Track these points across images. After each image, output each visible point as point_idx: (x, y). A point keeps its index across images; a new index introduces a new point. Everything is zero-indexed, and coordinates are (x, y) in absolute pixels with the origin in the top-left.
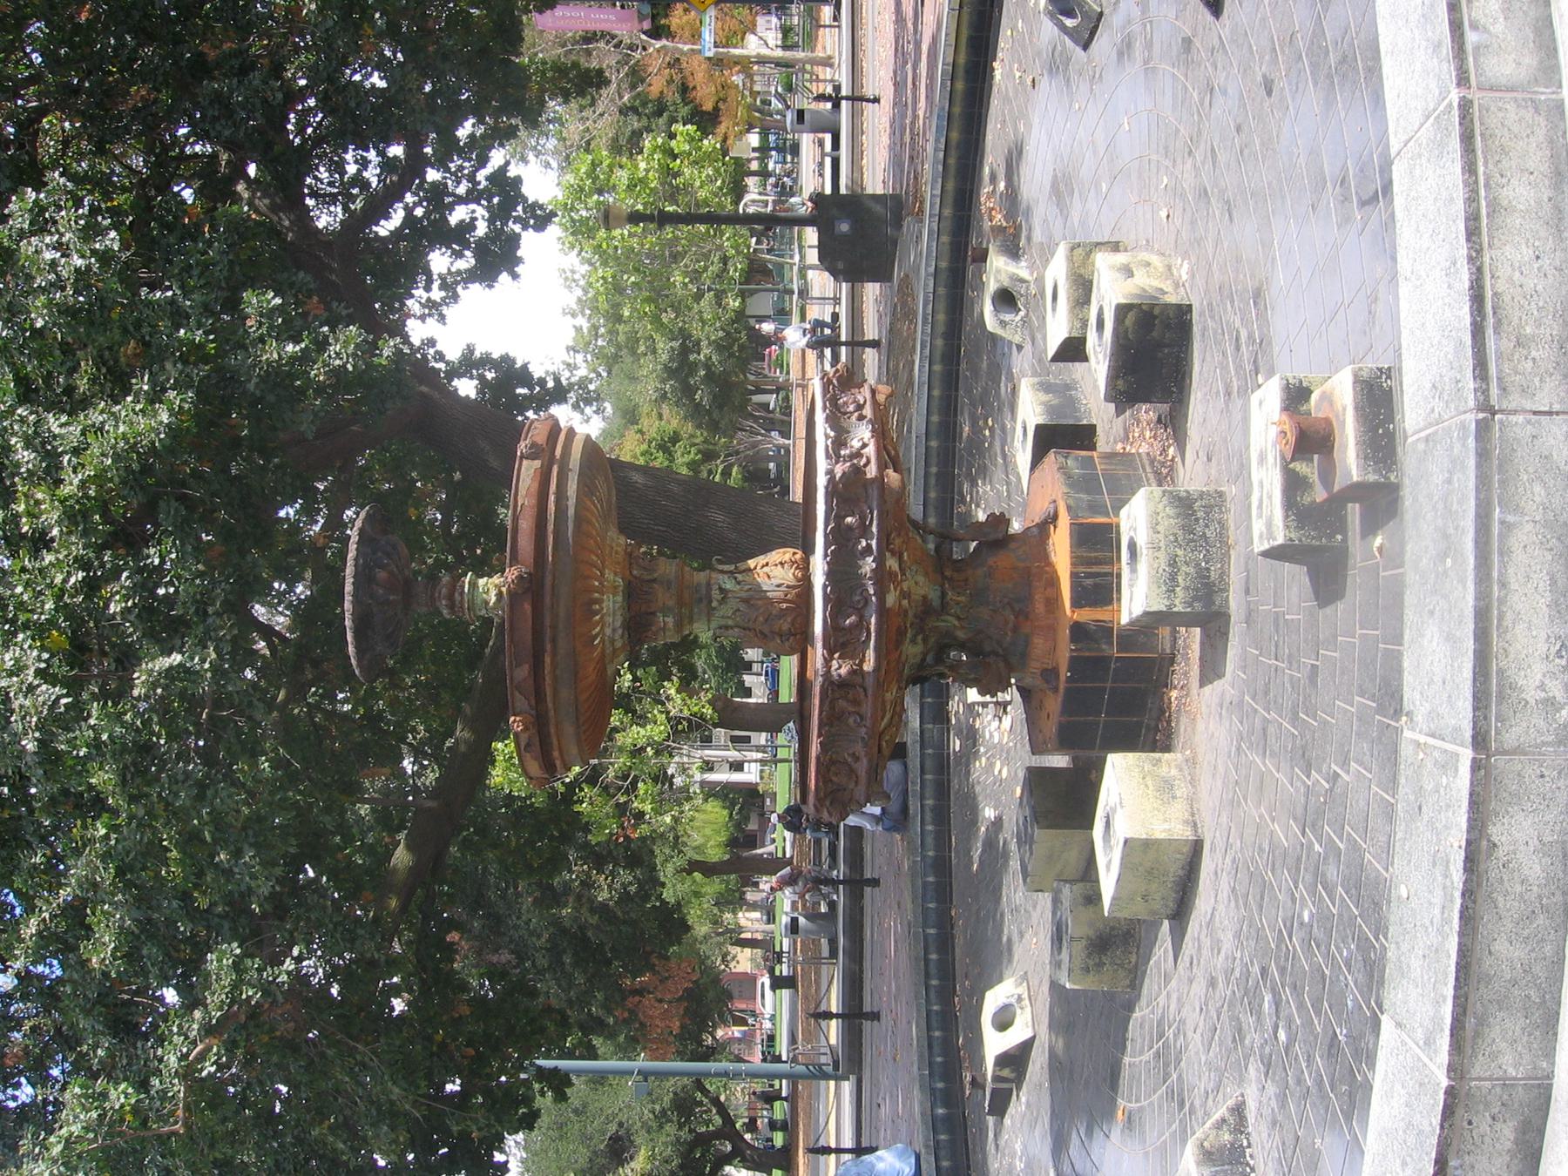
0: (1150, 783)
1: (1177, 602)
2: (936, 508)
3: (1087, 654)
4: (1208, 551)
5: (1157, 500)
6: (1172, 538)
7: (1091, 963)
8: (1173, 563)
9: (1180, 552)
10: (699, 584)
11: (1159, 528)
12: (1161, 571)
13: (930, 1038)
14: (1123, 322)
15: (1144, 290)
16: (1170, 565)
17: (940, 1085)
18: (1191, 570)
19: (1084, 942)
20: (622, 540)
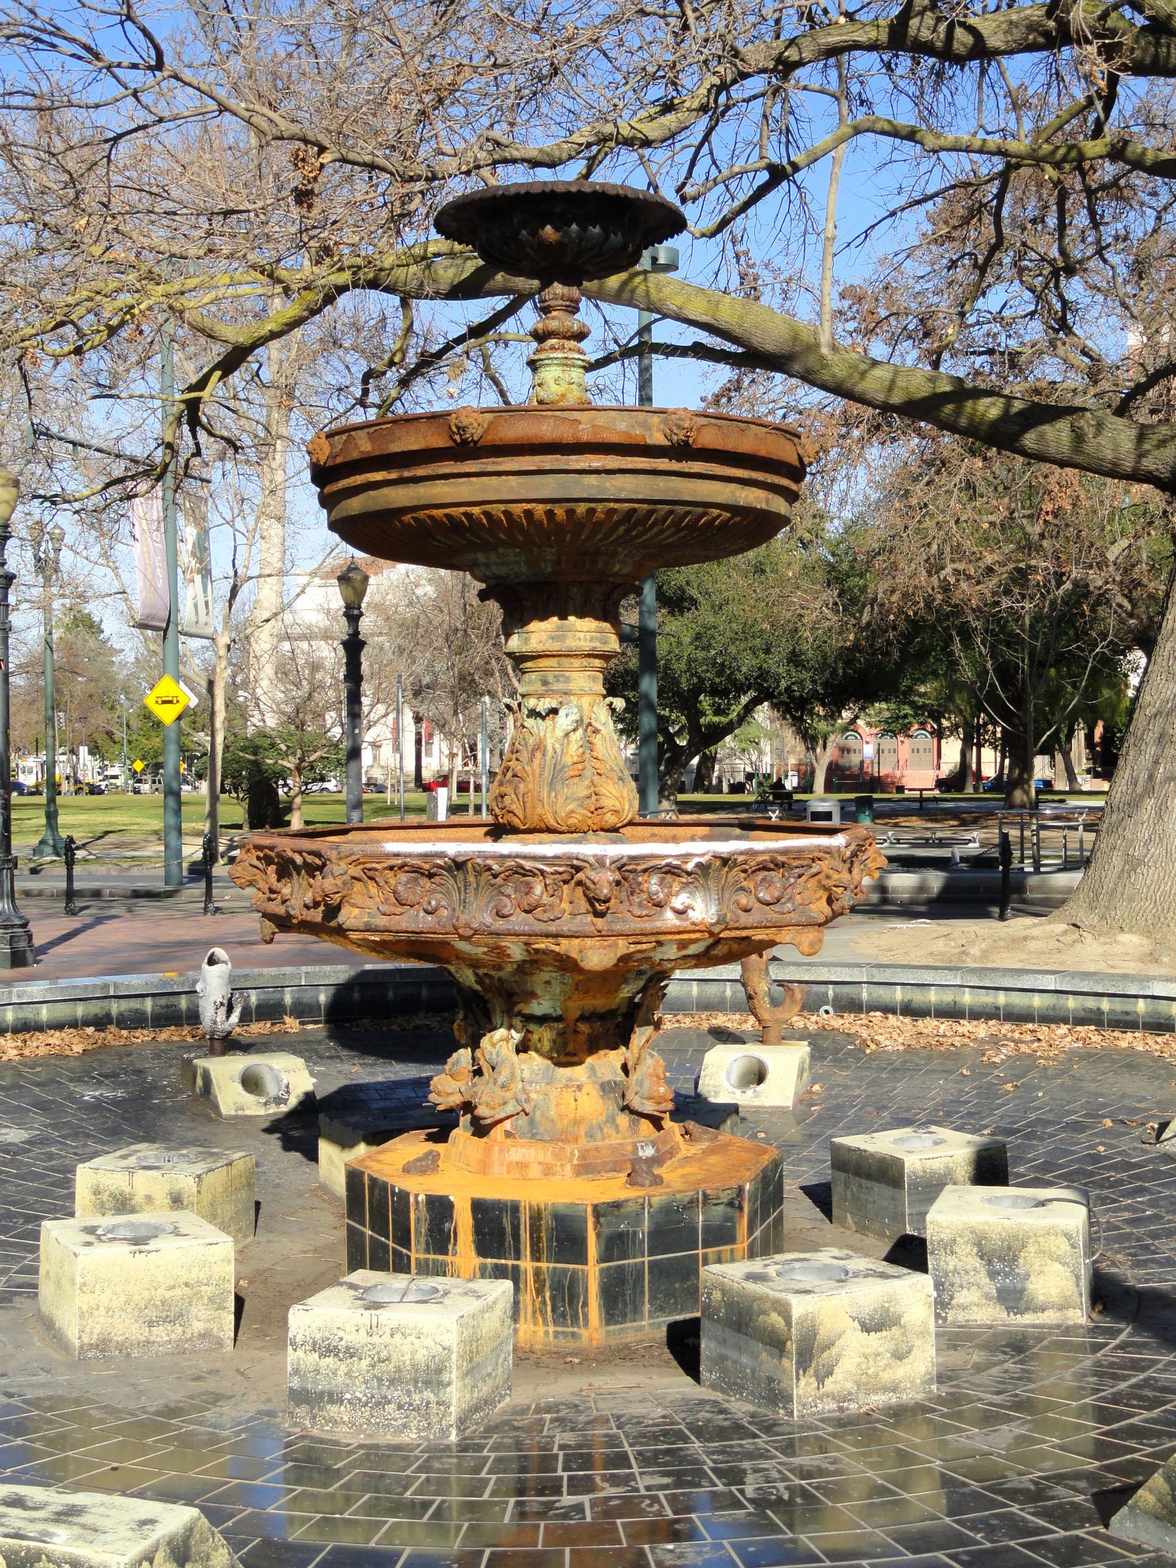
0: (178, 1292)
1: (300, 1353)
2: (1054, 1008)
3: (412, 1216)
4: (366, 1405)
6: (384, 1354)
7: (105, 1197)
8: (351, 1353)
9: (365, 1363)
10: (568, 680)
11: (398, 1337)
12: (340, 1334)
14: (775, 1309)
15: (828, 1346)
16: (348, 1348)
17: (424, 993)
18: (340, 1379)
19: (127, 1190)
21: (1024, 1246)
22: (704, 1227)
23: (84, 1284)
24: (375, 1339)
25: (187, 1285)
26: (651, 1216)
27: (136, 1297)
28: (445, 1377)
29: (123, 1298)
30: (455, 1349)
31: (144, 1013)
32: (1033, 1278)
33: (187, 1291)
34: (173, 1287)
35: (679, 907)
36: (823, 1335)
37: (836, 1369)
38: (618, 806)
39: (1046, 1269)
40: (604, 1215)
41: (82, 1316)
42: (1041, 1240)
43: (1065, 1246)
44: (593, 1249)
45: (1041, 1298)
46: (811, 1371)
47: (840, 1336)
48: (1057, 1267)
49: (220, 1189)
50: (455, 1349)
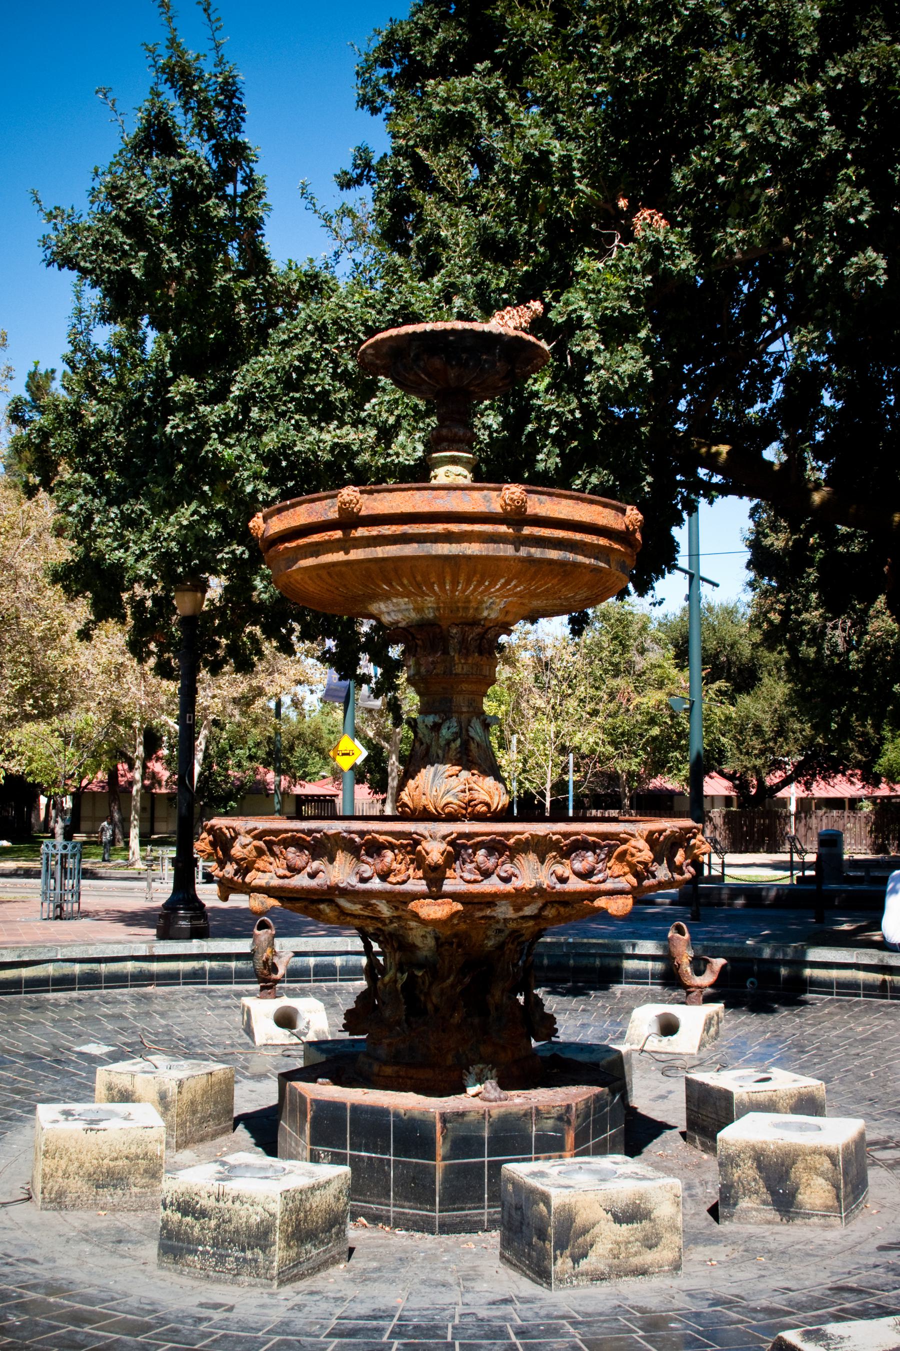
0: (120, 1163)
1: (169, 1212)
5: (267, 1206)
6: (227, 1216)
8: (203, 1214)
9: (213, 1223)
11: (238, 1203)
12: (197, 1198)
13: (594, 955)
15: (585, 1231)
19: (130, 1088)
20: (365, 671)
21: (794, 1163)
22: (537, 1136)
23: (47, 1151)
24: (221, 1204)
25: (127, 1158)
26: (491, 1125)
27: (87, 1165)
28: (271, 1237)
29: (76, 1164)
30: (278, 1215)
31: (334, 967)
32: (801, 1190)
33: (126, 1161)
34: (116, 1159)
35: (503, 874)
36: (580, 1221)
37: (590, 1253)
38: (487, 799)
39: (812, 1183)
40: (450, 1122)
41: (44, 1176)
42: (809, 1158)
43: (827, 1164)
44: (441, 1149)
45: (808, 1206)
46: (568, 1252)
47: (594, 1225)
48: (821, 1181)
49: (200, 1092)
50: (278, 1215)
